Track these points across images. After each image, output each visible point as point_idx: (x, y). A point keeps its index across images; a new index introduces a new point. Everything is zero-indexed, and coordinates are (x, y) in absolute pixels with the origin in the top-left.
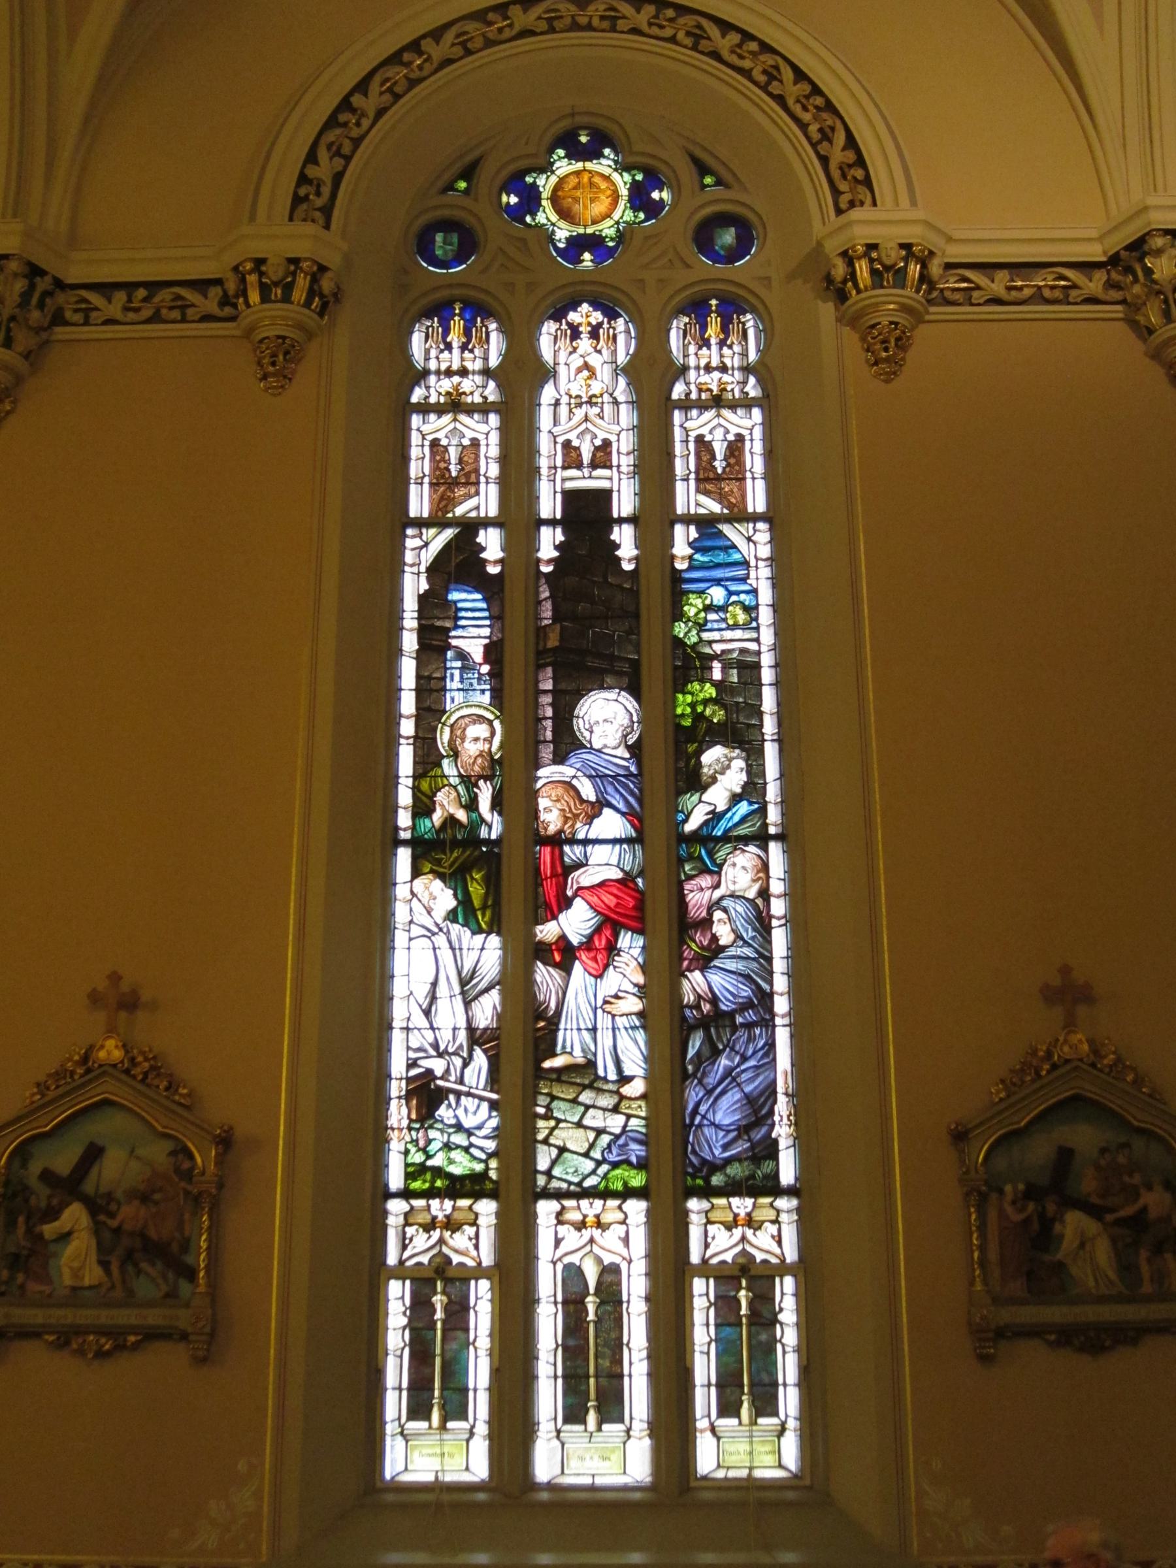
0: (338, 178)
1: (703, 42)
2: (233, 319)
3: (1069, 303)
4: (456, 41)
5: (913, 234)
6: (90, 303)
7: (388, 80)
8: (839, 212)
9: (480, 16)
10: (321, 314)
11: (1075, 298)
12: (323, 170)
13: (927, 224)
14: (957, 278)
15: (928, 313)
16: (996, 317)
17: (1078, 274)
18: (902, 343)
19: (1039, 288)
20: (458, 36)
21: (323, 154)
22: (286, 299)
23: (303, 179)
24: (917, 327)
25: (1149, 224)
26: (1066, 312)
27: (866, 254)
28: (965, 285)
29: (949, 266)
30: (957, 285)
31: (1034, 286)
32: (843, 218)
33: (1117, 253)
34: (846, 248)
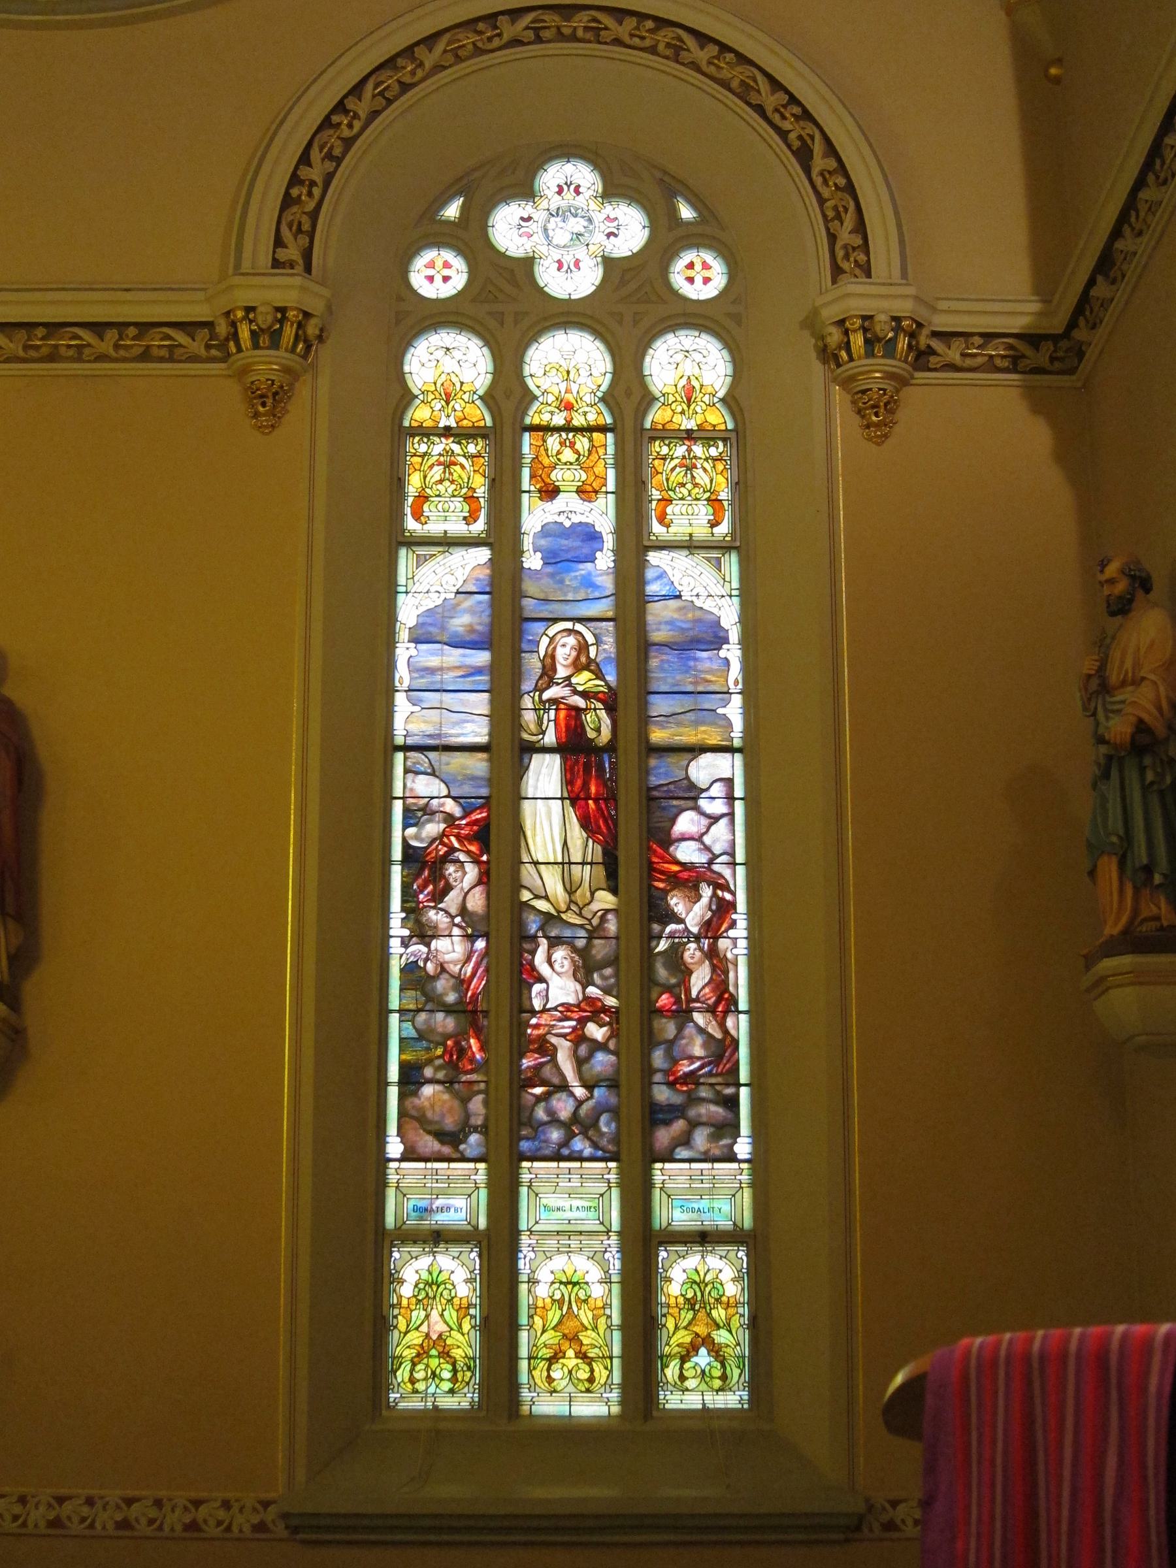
1: (683, 54)
2: (223, 360)
5: (904, 307)
6: (174, 340)
10: (305, 356)
13: (917, 298)
14: (161, 336)
15: (912, 378)
16: (951, 382)
17: (940, 343)
18: (891, 406)
19: (991, 357)
22: (275, 344)
23: (295, 180)
24: (901, 389)
27: (246, 317)
29: (935, 334)
30: (162, 343)
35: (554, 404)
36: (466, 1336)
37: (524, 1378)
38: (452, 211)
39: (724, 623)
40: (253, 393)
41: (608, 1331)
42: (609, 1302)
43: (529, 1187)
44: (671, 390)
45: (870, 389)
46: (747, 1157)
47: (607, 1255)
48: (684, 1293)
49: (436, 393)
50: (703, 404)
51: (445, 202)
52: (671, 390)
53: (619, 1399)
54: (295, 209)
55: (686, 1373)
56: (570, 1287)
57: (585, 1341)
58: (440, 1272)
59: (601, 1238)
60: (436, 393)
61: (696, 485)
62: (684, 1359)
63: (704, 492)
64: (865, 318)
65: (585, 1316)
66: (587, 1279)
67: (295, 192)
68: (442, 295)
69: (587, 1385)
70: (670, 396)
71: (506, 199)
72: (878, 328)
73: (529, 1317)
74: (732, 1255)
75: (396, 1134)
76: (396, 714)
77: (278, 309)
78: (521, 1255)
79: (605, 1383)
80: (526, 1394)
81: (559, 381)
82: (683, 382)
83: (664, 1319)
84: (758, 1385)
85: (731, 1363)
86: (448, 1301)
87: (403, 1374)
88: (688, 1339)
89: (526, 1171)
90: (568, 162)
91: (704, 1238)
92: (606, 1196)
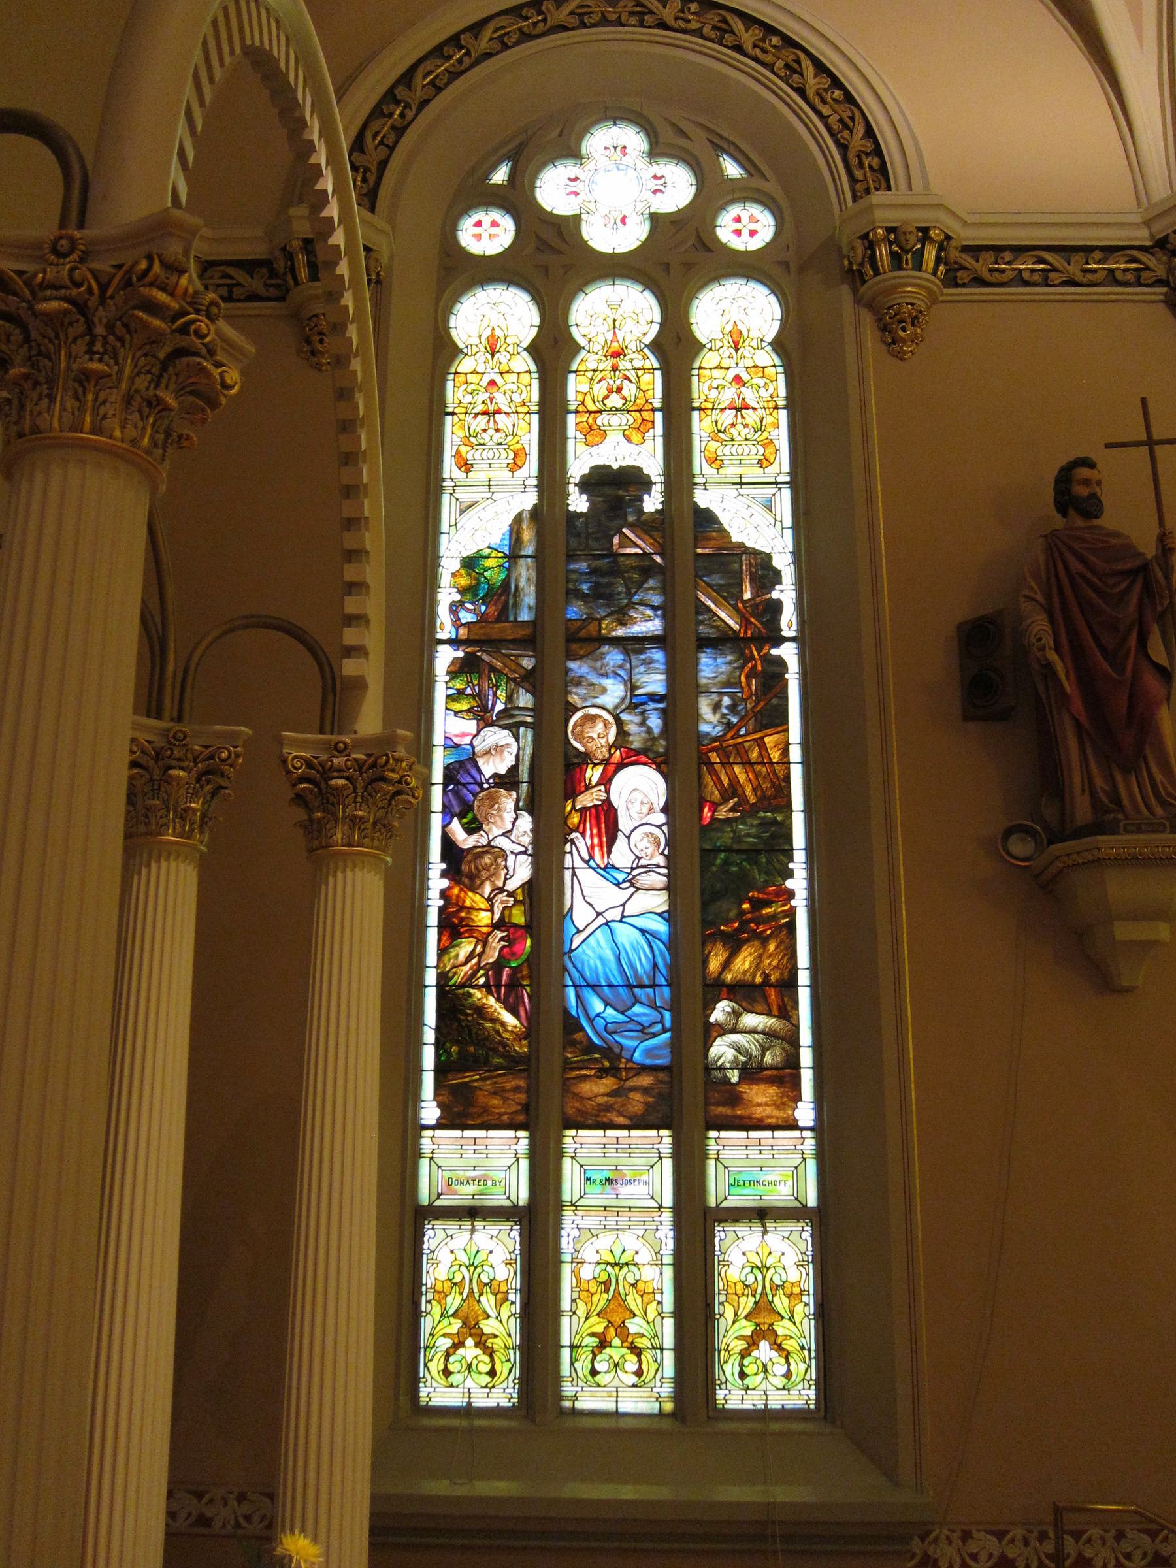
2: (282, 299)
3: (1140, 285)
4: (495, 36)
7: (431, 72)
8: (855, 198)
9: (515, 11)
11: (1145, 279)
14: (1035, 259)
15: (942, 294)
19: (1020, 271)
20: (495, 31)
26: (975, 294)
28: (1042, 266)
29: (966, 249)
31: (1015, 269)
32: (862, 203)
33: (1167, 236)
35: (600, 353)
36: (652, 1324)
37: (565, 1369)
38: (500, 176)
40: (890, 318)
41: (659, 1318)
42: (807, 1289)
43: (717, 1159)
44: (475, 341)
46: (811, 1124)
47: (658, 1234)
48: (596, 1276)
49: (480, 346)
51: (494, 167)
52: (475, 341)
53: (672, 1395)
55: (746, 1370)
56: (617, 1268)
57: (780, 1331)
58: (478, 1252)
59: (654, 1214)
60: (480, 346)
61: (746, 426)
62: (744, 1354)
63: (755, 432)
64: (890, 230)
65: (633, 1301)
66: (638, 1259)
68: (750, 248)
69: (488, 1379)
71: (552, 160)
73: (572, 1301)
74: (503, 1235)
75: (432, 1098)
76: (437, 660)
78: (563, 1233)
79: (803, 1379)
80: (568, 1389)
81: (605, 331)
82: (488, 332)
83: (721, 1307)
84: (824, 1383)
85: (499, 1357)
86: (633, 1285)
87: (436, 1366)
88: (748, 1332)
89: (712, 1142)
90: (615, 124)
91: (762, 1215)
92: (657, 1167)
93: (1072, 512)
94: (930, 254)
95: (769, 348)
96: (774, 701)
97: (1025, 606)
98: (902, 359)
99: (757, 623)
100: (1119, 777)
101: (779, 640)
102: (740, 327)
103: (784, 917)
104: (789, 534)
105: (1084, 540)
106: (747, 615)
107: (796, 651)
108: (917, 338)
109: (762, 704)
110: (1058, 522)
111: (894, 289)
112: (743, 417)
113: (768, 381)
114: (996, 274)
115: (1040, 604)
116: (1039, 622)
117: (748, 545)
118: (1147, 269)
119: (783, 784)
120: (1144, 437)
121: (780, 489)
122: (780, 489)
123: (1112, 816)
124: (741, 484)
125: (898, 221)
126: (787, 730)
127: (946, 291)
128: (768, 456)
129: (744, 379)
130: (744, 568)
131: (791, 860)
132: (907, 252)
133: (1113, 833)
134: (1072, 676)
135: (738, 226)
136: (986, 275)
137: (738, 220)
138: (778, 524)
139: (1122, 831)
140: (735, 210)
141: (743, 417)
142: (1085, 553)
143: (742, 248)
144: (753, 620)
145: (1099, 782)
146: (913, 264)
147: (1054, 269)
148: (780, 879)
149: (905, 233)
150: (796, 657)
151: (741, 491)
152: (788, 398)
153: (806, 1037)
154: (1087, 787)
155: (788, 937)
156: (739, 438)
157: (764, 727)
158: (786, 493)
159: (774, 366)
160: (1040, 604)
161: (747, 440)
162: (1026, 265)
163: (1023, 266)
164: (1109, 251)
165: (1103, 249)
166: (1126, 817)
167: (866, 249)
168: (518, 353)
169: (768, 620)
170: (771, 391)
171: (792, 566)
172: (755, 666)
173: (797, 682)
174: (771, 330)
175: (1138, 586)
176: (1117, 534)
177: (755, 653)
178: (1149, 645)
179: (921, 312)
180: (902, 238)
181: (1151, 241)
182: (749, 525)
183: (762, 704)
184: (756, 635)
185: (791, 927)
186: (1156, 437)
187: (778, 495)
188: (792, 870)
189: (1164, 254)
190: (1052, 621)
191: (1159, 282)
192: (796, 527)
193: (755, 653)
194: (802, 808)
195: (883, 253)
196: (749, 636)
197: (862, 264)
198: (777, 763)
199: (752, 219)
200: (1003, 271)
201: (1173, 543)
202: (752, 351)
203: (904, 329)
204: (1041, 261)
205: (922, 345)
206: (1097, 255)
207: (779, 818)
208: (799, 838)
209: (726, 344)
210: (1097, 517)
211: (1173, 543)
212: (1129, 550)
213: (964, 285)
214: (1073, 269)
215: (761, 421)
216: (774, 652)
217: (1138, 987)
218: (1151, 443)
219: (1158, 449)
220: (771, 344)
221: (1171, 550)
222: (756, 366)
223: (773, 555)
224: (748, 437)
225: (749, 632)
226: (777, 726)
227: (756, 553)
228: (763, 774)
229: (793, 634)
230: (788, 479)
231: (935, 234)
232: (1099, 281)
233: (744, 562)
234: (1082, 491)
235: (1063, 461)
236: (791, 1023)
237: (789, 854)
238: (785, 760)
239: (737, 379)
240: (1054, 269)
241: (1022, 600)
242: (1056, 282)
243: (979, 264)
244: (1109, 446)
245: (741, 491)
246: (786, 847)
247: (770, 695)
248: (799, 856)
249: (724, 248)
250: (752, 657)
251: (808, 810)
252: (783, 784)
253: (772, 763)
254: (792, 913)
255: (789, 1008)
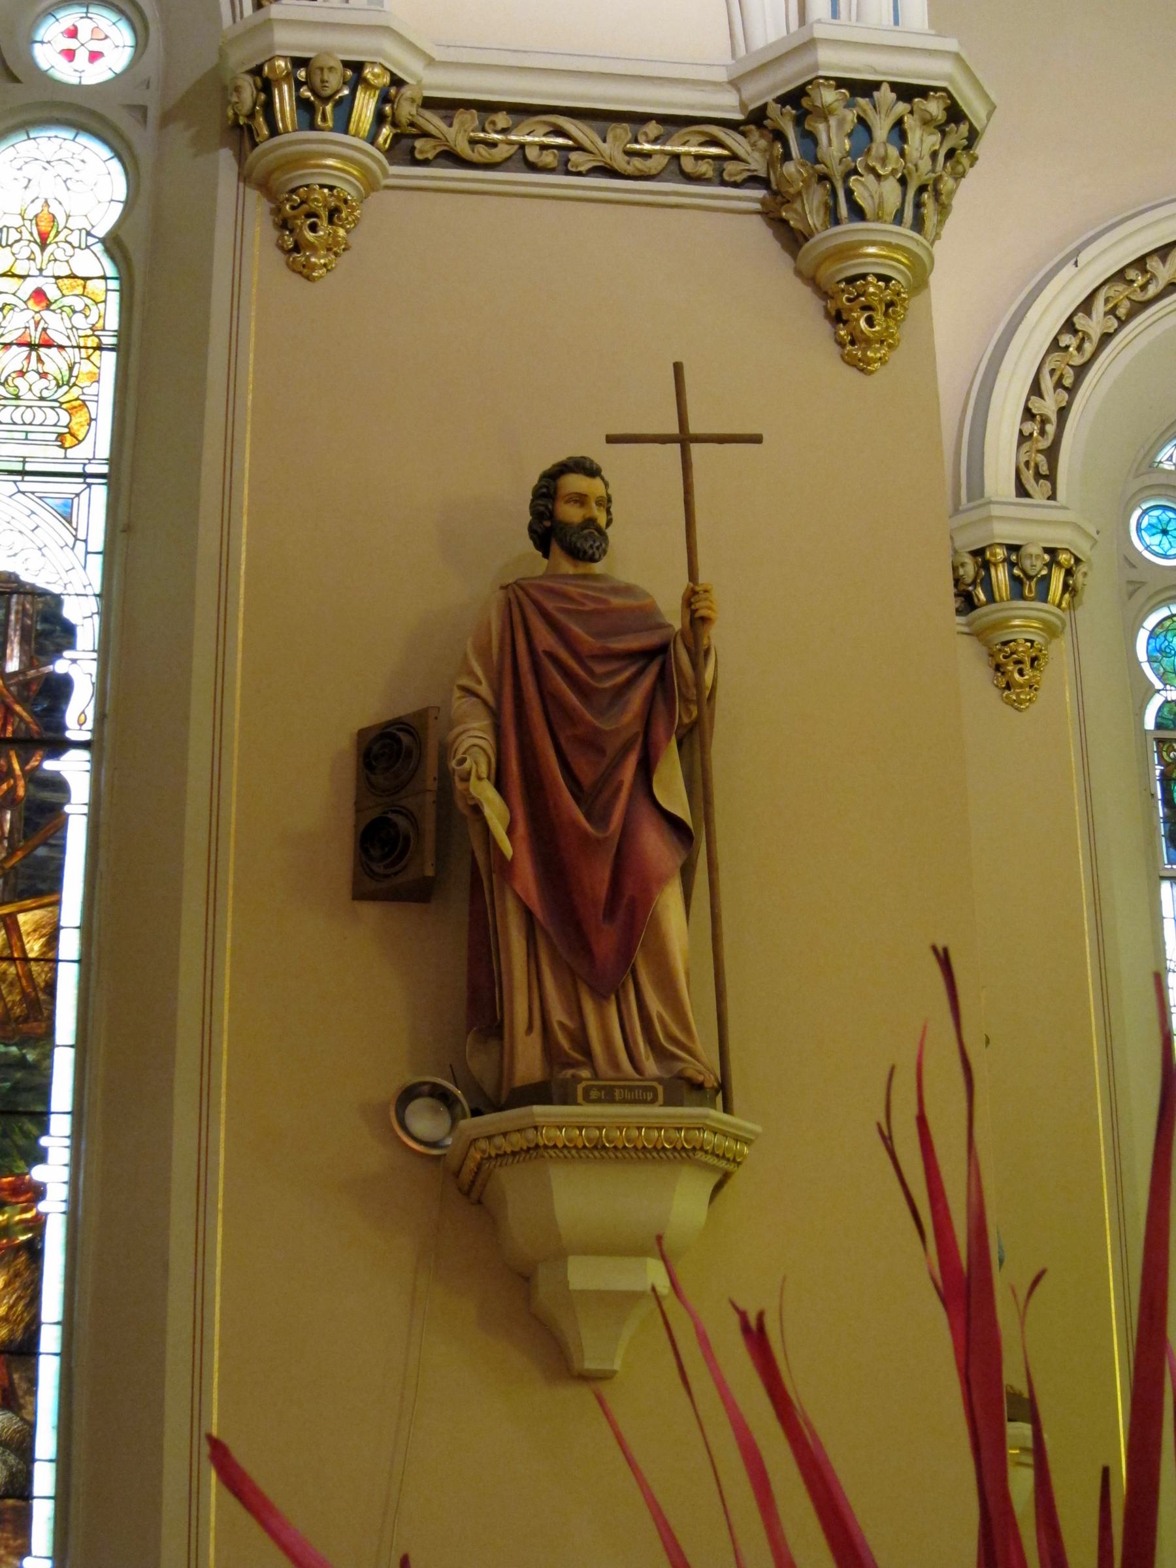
0: (1106, 338)
3: (724, 183)
11: (730, 175)
12: (1094, 325)
13: (957, 57)
14: (702, 139)
15: (386, 175)
19: (522, 146)
21: (1099, 307)
23: (1069, 326)
25: (816, 67)
29: (429, 103)
33: (764, 107)
34: (259, 62)
39: (72, 611)
40: (293, 208)
45: (1014, 641)
50: (67, 246)
54: (1120, 287)
61: (43, 375)
63: (59, 386)
64: (299, 62)
67: (1131, 274)
68: (87, 81)
70: (12, 231)
72: (1027, 564)
77: (1047, 550)
93: (555, 549)
94: (365, 107)
95: (99, 248)
96: (42, 852)
97: (461, 704)
98: (309, 278)
99: (25, 714)
100: (588, 1006)
101: (59, 746)
102: (55, 209)
103: (24, 1232)
104: (96, 563)
105: (565, 596)
106: (9, 700)
107: (88, 766)
108: (337, 244)
109: (20, 854)
110: (538, 565)
111: (300, 161)
112: (39, 360)
113: (89, 302)
114: (481, 148)
115: (485, 702)
116: (472, 733)
117: (25, 577)
118: (735, 157)
119: (42, 997)
120: (674, 429)
121: (89, 485)
122: (89, 485)
123: (569, 1073)
124: (23, 473)
125: (311, 50)
126: (58, 903)
127: (394, 170)
128: (75, 427)
129: (50, 296)
130: (13, 617)
131: (45, 1130)
132: (326, 100)
133: (564, 1102)
134: (521, 829)
135: (71, 44)
136: (463, 149)
137: (73, 33)
138: (80, 546)
139: (580, 1099)
140: (69, 17)
141: (39, 360)
142: (562, 618)
143: (73, 80)
144: (18, 708)
145: (558, 1014)
146: (335, 120)
147: (580, 148)
148: (22, 1164)
149: (322, 69)
150: (87, 776)
151: (23, 487)
152: (124, 332)
153: (46, 1443)
154: (537, 1023)
155: (27, 1267)
156: (29, 396)
157: (21, 895)
158: (100, 493)
159: (104, 278)
160: (485, 702)
161: (42, 399)
162: (532, 136)
163: (529, 139)
164: (674, 123)
165: (663, 120)
166: (596, 1075)
167: (259, 90)
168: (88, 247)
169: (44, 710)
170: (93, 319)
171: (96, 618)
172: (13, 789)
173: (84, 819)
174: (106, 219)
175: (647, 681)
176: (627, 590)
177: (16, 766)
178: (655, 778)
179: (346, 201)
180: (317, 80)
181: (742, 111)
182: (30, 544)
183: (20, 854)
184: (22, 735)
185: (34, 1252)
186: (694, 428)
187: (84, 496)
188: (45, 1151)
189: (762, 136)
190: (498, 731)
191: (754, 180)
192: (108, 554)
193: (16, 766)
194: (72, 1041)
195: (1001, 576)
196: (9, 734)
197: (251, 115)
198: (36, 960)
199: (98, 35)
200: (493, 145)
201: (710, 608)
202: (70, 250)
203: (313, 228)
204: (559, 132)
205: (345, 256)
206: (653, 129)
207: (31, 1057)
208: (62, 1094)
209: (26, 235)
210: (593, 559)
211: (710, 608)
212: (647, 617)
213: (425, 163)
214: (611, 149)
215: (71, 369)
216: (49, 765)
217: (615, 1372)
218: (684, 439)
219: (695, 449)
220: (103, 241)
221: (705, 620)
222: (73, 276)
223: (65, 598)
224: (45, 394)
225: (10, 729)
226: (38, 894)
227: (35, 593)
228: (10, 978)
229: (86, 736)
230: (105, 469)
231: (374, 75)
232: (654, 172)
233: (14, 608)
234: (571, 514)
235: (548, 463)
236: (22, 1419)
237: (42, 1120)
238: (50, 955)
239: (39, 295)
240: (580, 148)
241: (457, 693)
242: (583, 169)
243: (453, 130)
244: (612, 439)
245: (23, 487)
246: (40, 1108)
247: (36, 841)
248: (60, 1125)
249: (44, 77)
250: (10, 772)
251: (82, 1045)
252: (42, 997)
253: (25, 960)
254: (38, 1225)
255: (20, 1393)
